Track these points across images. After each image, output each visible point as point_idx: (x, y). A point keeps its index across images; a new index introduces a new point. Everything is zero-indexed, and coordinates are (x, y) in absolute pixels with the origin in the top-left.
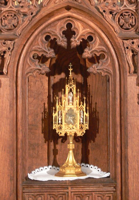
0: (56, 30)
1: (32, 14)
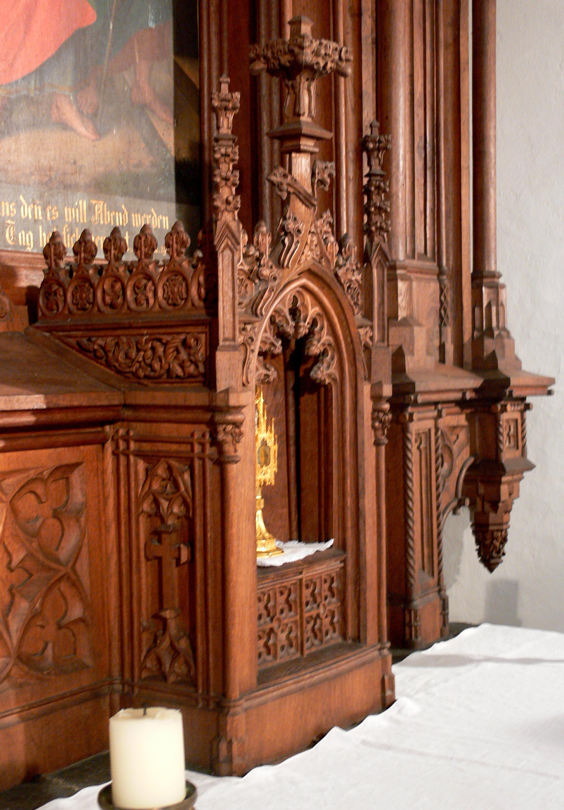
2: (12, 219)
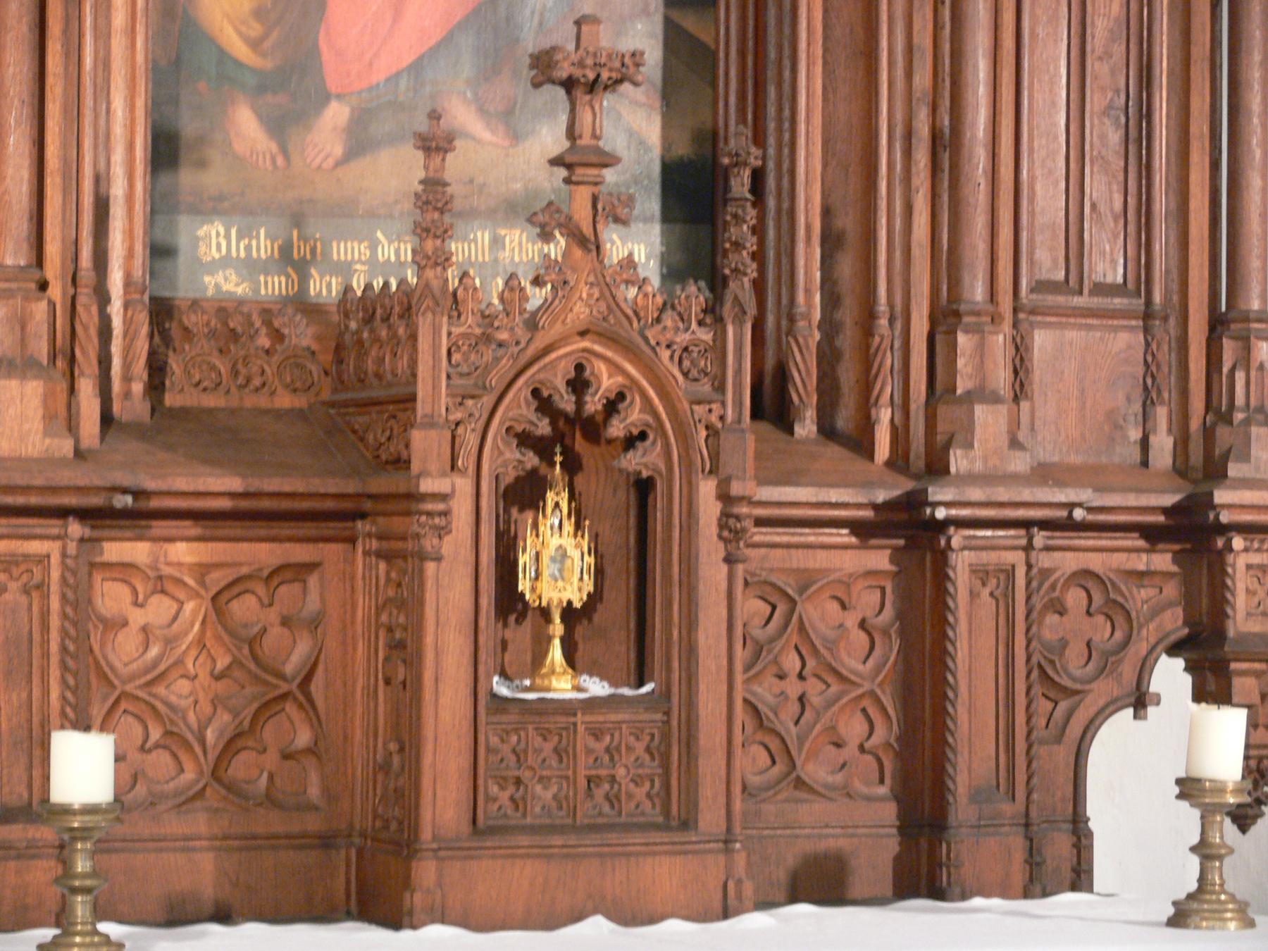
0: (556, 375)
1: (518, 343)
2: (363, 263)
